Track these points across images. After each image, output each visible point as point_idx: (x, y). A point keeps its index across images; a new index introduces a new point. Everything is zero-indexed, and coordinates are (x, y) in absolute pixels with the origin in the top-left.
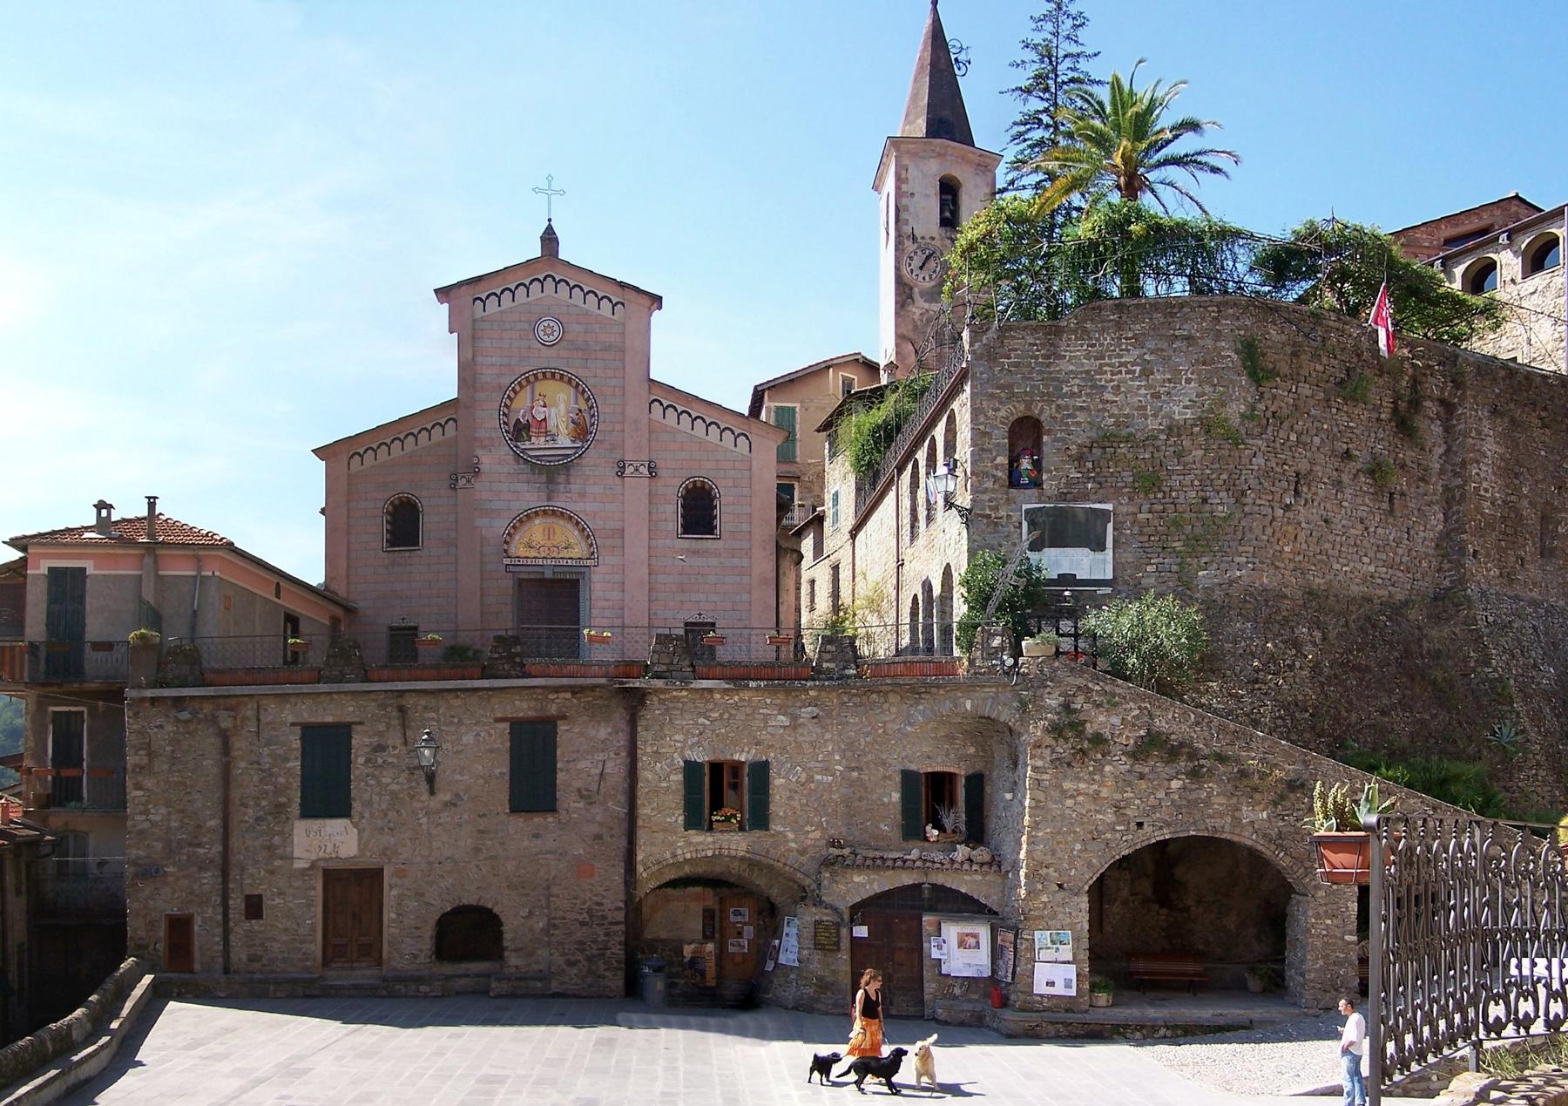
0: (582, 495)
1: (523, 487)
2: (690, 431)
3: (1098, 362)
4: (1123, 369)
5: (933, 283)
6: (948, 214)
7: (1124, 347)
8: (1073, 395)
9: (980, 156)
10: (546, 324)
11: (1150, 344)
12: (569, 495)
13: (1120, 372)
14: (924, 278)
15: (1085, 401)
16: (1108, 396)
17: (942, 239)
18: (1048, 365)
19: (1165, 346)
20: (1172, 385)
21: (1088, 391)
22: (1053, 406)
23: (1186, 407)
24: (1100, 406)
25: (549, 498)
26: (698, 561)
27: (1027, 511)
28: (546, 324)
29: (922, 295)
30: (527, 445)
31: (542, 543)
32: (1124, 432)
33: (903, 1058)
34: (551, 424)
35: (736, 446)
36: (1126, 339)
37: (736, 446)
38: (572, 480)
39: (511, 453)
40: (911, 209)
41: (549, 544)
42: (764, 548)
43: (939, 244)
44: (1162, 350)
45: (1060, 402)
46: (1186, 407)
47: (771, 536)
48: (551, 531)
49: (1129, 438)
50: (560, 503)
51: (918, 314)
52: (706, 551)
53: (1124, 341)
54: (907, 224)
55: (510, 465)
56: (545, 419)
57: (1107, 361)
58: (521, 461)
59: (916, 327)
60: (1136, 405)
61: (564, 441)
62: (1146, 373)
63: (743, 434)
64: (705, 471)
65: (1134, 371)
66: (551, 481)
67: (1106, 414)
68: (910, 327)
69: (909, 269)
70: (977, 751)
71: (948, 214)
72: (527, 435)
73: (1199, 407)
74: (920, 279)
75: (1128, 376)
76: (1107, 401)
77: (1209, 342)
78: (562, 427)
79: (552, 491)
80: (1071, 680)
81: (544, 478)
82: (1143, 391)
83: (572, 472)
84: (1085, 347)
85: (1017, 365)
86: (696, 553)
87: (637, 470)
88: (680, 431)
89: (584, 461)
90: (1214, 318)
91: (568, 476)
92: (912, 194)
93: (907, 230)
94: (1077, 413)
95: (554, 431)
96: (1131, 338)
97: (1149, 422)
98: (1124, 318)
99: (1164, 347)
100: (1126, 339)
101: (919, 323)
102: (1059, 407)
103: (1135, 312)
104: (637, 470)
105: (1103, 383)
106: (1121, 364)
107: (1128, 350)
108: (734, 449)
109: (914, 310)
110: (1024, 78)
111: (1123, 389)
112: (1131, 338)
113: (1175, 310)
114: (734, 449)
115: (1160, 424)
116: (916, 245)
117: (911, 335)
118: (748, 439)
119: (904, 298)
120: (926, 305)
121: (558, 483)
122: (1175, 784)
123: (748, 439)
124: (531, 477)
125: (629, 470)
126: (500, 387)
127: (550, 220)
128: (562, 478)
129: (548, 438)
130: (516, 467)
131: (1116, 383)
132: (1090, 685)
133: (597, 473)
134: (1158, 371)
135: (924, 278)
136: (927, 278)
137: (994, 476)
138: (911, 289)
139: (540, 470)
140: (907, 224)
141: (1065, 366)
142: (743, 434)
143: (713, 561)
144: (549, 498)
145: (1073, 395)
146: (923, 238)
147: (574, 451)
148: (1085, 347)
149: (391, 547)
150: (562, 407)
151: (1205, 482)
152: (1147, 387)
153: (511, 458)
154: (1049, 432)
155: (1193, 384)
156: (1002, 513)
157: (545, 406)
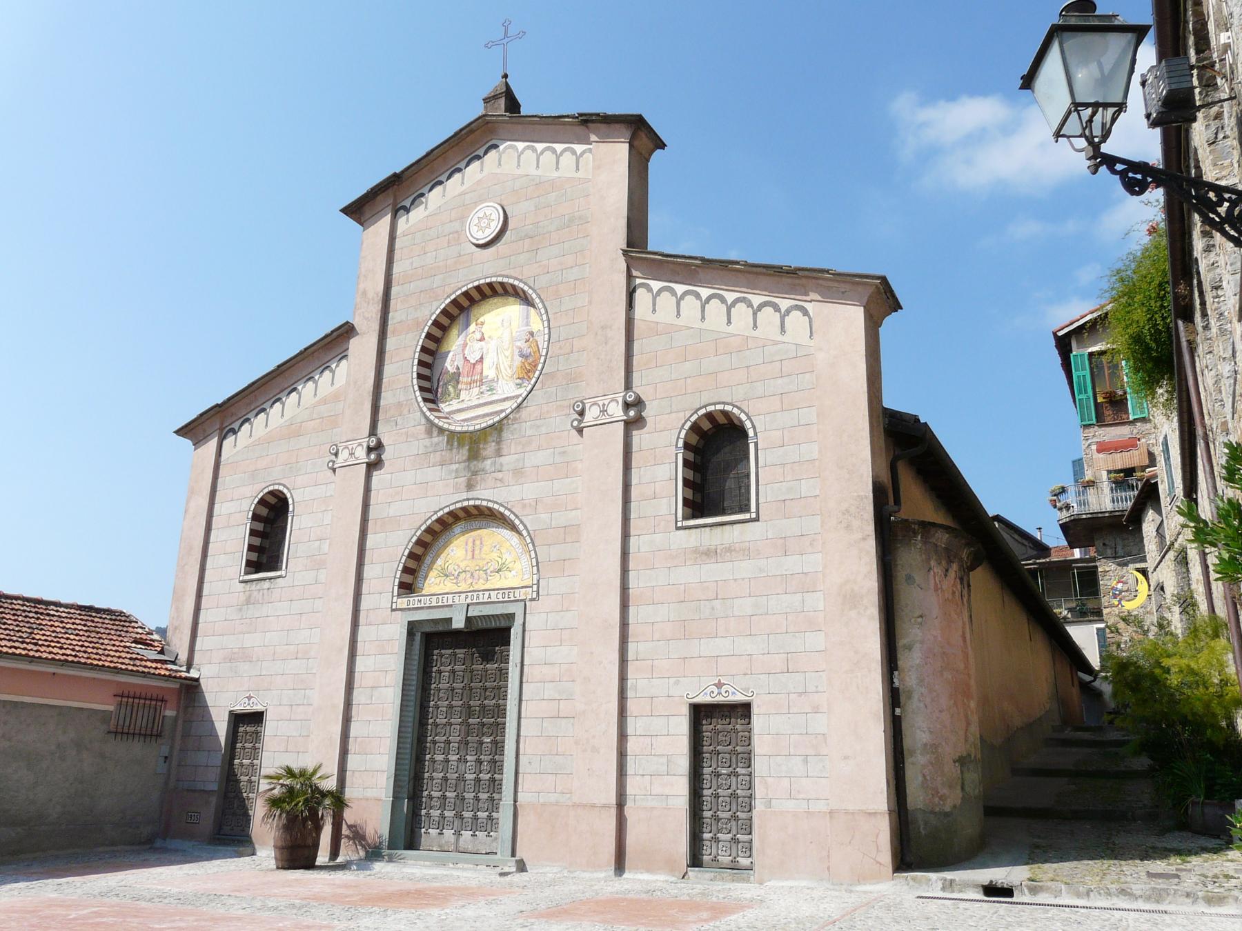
0: (518, 472)
1: (433, 473)
10: (481, 214)
12: (500, 475)
25: (470, 486)
26: (713, 571)
31: (463, 565)
33: (899, 310)
34: (489, 371)
38: (505, 451)
39: (423, 421)
41: (472, 566)
42: (848, 527)
47: (861, 498)
48: (478, 542)
50: (486, 495)
52: (729, 550)
61: (508, 388)
66: (474, 455)
72: (455, 388)
79: (475, 473)
81: (464, 452)
83: (505, 434)
86: (709, 554)
87: (604, 411)
89: (524, 414)
91: (499, 443)
104: (604, 411)
114: (780, 338)
118: (805, 312)
121: (485, 459)
123: (805, 312)
124: (447, 454)
125: (591, 414)
126: (418, 324)
127: (506, 76)
128: (490, 449)
129: (484, 388)
130: (427, 442)
143: (745, 568)
144: (470, 486)
149: (694, 517)
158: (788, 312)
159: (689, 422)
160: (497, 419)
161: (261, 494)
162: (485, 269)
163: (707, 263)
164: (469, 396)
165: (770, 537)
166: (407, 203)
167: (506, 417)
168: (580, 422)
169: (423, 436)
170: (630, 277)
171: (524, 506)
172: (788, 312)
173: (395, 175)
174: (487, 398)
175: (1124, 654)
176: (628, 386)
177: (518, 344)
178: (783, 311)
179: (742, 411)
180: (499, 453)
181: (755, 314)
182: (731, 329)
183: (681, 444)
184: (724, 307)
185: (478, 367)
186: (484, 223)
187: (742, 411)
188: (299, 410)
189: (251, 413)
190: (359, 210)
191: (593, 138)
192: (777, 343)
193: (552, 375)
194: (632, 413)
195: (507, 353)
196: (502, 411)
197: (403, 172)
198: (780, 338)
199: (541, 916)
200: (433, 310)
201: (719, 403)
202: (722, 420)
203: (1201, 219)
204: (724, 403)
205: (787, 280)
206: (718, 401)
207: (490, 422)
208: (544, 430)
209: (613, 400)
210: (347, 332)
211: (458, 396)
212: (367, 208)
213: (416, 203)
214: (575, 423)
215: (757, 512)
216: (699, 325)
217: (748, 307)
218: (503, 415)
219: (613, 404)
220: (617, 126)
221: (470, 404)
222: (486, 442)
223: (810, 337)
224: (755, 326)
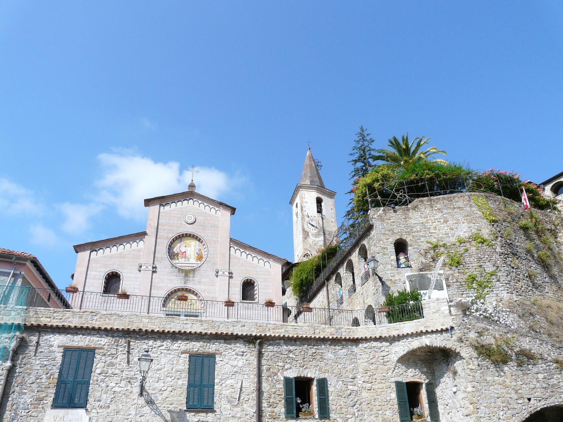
0: (200, 282)
1: (174, 278)
2: (246, 259)
3: (426, 219)
4: (436, 221)
5: (316, 231)
6: (319, 210)
7: (434, 213)
8: (418, 232)
9: (329, 192)
10: (189, 215)
11: (445, 211)
12: (194, 282)
13: (435, 222)
14: (313, 230)
15: (423, 233)
16: (432, 231)
17: (318, 217)
18: (406, 221)
19: (451, 211)
20: (457, 225)
21: (424, 230)
22: (411, 236)
23: (465, 232)
24: (430, 235)
25: (185, 283)
27: (408, 277)
28: (189, 215)
29: (312, 235)
30: (177, 261)
32: (441, 243)
35: (264, 266)
36: (435, 210)
37: (264, 266)
38: (196, 276)
39: (170, 264)
40: (307, 207)
43: (317, 218)
44: (450, 213)
45: (413, 234)
46: (465, 232)
49: (444, 245)
50: (189, 286)
51: (311, 241)
53: (434, 211)
54: (305, 212)
55: (169, 269)
56: (185, 252)
57: (429, 218)
58: (174, 267)
59: (311, 246)
60: (444, 233)
61: (193, 260)
62: (446, 221)
63: (267, 261)
64: (251, 276)
65: (440, 221)
67: (433, 237)
68: (309, 246)
69: (307, 226)
70: (427, 371)
71: (319, 210)
72: (177, 257)
73: (470, 232)
74: (311, 229)
75: (439, 223)
76: (432, 233)
77: (468, 209)
78: (192, 255)
80: (479, 324)
81: (183, 274)
82: (446, 228)
83: (196, 273)
84: (419, 214)
85: (394, 222)
87: (224, 273)
88: (241, 259)
89: (201, 269)
90: (468, 200)
91: (194, 274)
92: (307, 202)
93: (306, 213)
94: (421, 238)
95: (189, 257)
96: (437, 210)
97: (451, 239)
98: (433, 203)
99: (450, 212)
100: (435, 210)
101: (312, 245)
102: (413, 236)
103: (436, 200)
104: (224, 273)
105: (429, 226)
106: (435, 219)
107: (437, 214)
108: (264, 267)
109: (310, 240)
110: (356, 157)
111: (437, 228)
112: (437, 210)
113: (452, 199)
115: (456, 239)
116: (309, 219)
117: (309, 249)
118: (269, 263)
119: (306, 235)
120: (314, 239)
121: (189, 277)
122: (540, 376)
123: (269, 263)
124: (178, 274)
125: (220, 273)
126: (168, 238)
128: (191, 275)
129: (186, 259)
130: (172, 269)
131: (434, 226)
132: (488, 327)
133: (207, 274)
134: (450, 220)
135: (313, 230)
136: (314, 229)
137: (391, 264)
138: (308, 233)
139: (181, 271)
140: (305, 212)
141: (412, 221)
142: (267, 261)
145: (418, 232)
146: (311, 216)
147: (196, 265)
148: (419, 214)
150: (193, 248)
151: (479, 259)
152: (447, 226)
153: (170, 265)
154: (411, 246)
155: (465, 224)
156: (397, 278)
157: (186, 247)
158: (266, 262)
160: (193, 268)
161: (109, 272)
162: (189, 230)
163: (250, 247)
164: (181, 260)
166: (164, 204)
167: (196, 268)
168: (218, 274)
169: (170, 268)
170: (230, 244)
171: (201, 291)
172: (266, 262)
173: (164, 196)
174: (187, 262)
176: (153, 264)
177: (196, 251)
180: (194, 277)
181: (258, 260)
182: (253, 262)
183: (104, 277)
185: (185, 254)
186: (190, 218)
188: (124, 251)
191: (221, 208)
192: (263, 268)
193: (209, 261)
194: (154, 270)
195: (193, 252)
196: (194, 267)
197: (165, 196)
199: (547, 319)
200: (172, 235)
202: (252, 282)
205: (266, 255)
207: (191, 269)
208: (207, 274)
209: (150, 265)
210: (144, 234)
211: (178, 259)
212: (152, 202)
213: (167, 205)
214: (139, 269)
218: (195, 268)
219: (150, 266)
220: (229, 208)
221: (182, 262)
222: (190, 273)
224: (258, 263)
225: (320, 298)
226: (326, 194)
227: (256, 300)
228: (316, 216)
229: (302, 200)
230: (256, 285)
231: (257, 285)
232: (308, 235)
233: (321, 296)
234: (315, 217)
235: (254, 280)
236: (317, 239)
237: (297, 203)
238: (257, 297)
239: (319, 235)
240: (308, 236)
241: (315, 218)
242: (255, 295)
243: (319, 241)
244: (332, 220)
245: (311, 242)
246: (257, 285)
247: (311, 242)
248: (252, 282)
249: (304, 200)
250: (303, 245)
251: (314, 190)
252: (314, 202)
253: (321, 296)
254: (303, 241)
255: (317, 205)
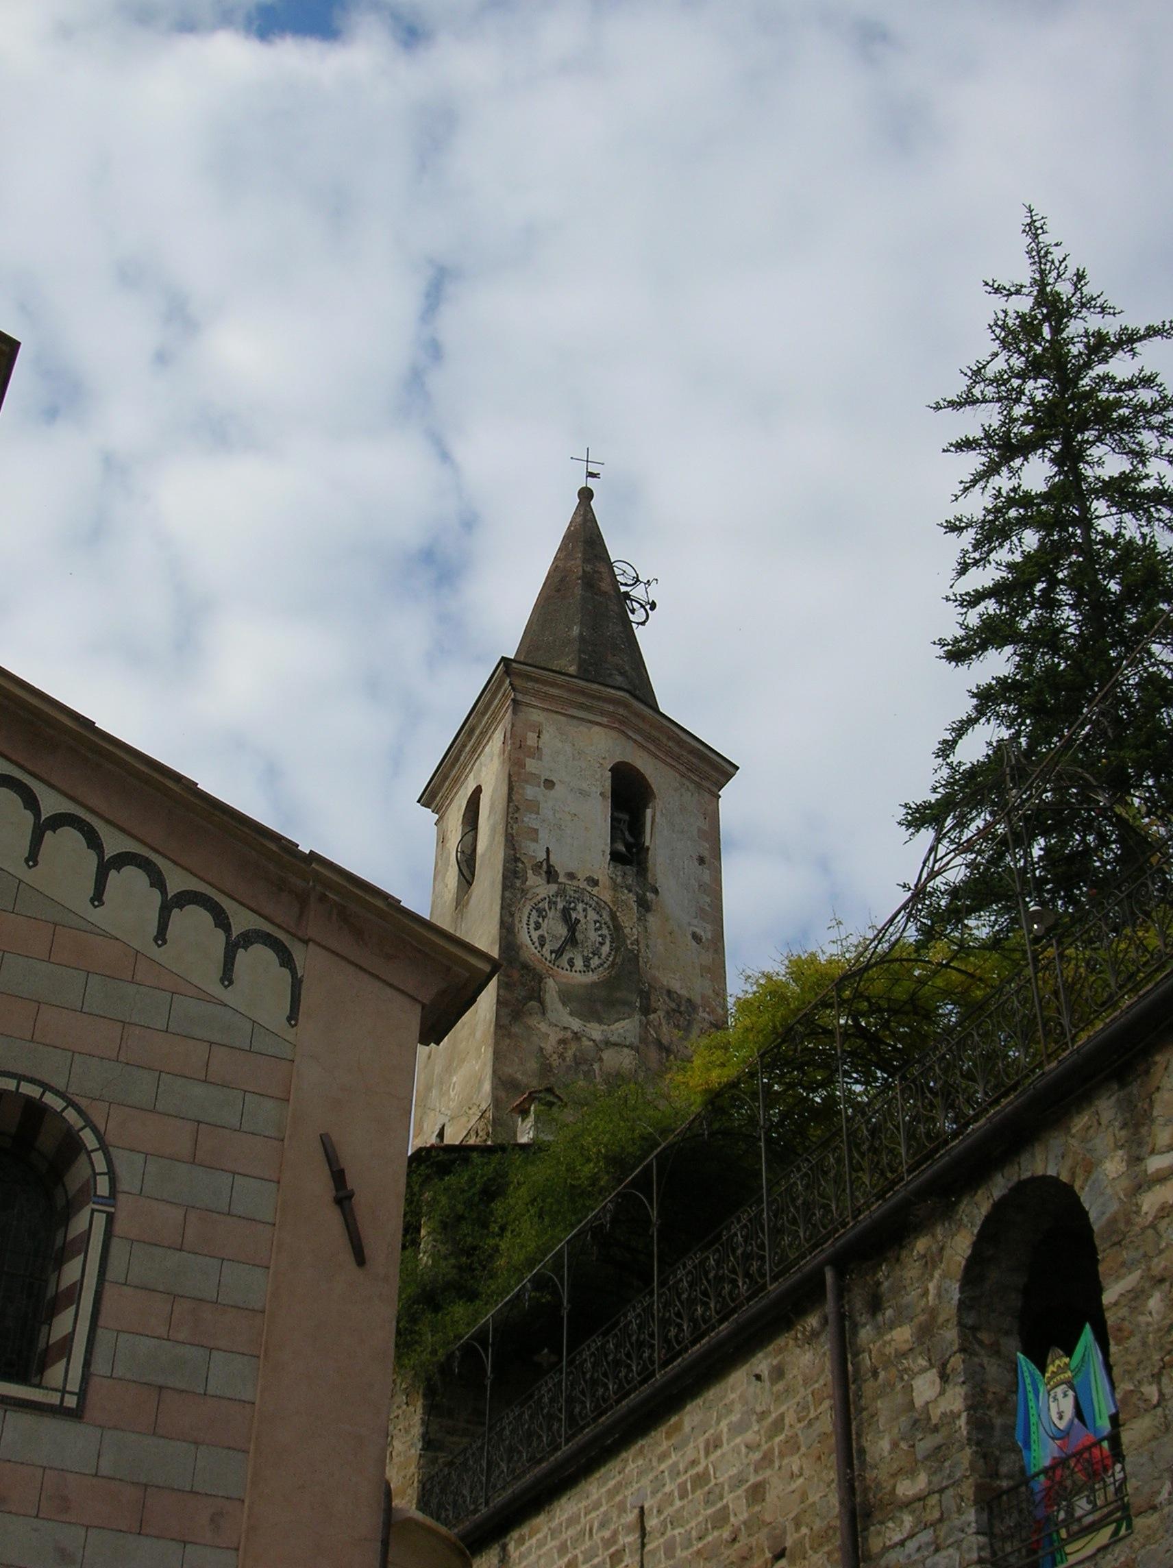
5: (591, 977)
17: (615, 887)
29: (566, 996)
43: (607, 896)
54: (536, 840)
68: (533, 1065)
69: (535, 935)
92: (549, 784)
101: (555, 1061)
109: (543, 1027)
114: (217, 990)
118: (286, 960)
119: (521, 992)
120: (576, 1024)
138: (540, 979)
140: (536, 840)
146: (571, 876)
159: (15, 1082)
165: (104, 1471)
175: (885, 1444)
178: (235, 933)
179: (90, 1124)
182: (96, 915)
184: (91, 861)
187: (90, 1124)
189: (122, 837)
190: (548, 848)
198: (217, 990)
201: (32, 1081)
203: (823, 959)
204: (46, 1087)
206: (28, 1074)
215: (82, 1394)
216: (21, 871)
217: (152, 885)
223: (289, 1019)
225: (714, 1445)
226: (677, 758)
227: (55, 1374)
228: (603, 878)
229: (522, 765)
230: (87, 1192)
231: (103, 1187)
232: (536, 995)
233: (737, 1429)
234: (595, 883)
235: (71, 1115)
236: (596, 1031)
237: (478, 790)
238: (68, 1340)
239: (610, 1003)
240: (541, 1002)
241: (595, 891)
242: (55, 1307)
243: (608, 1044)
244: (699, 931)
245: (550, 1045)
246: (103, 1187)
247: (550, 1045)
248: (47, 1141)
249: (531, 765)
250: (498, 1056)
251: (603, 713)
252: (596, 790)
253: (737, 1429)
254: (498, 1026)
255: (613, 819)
